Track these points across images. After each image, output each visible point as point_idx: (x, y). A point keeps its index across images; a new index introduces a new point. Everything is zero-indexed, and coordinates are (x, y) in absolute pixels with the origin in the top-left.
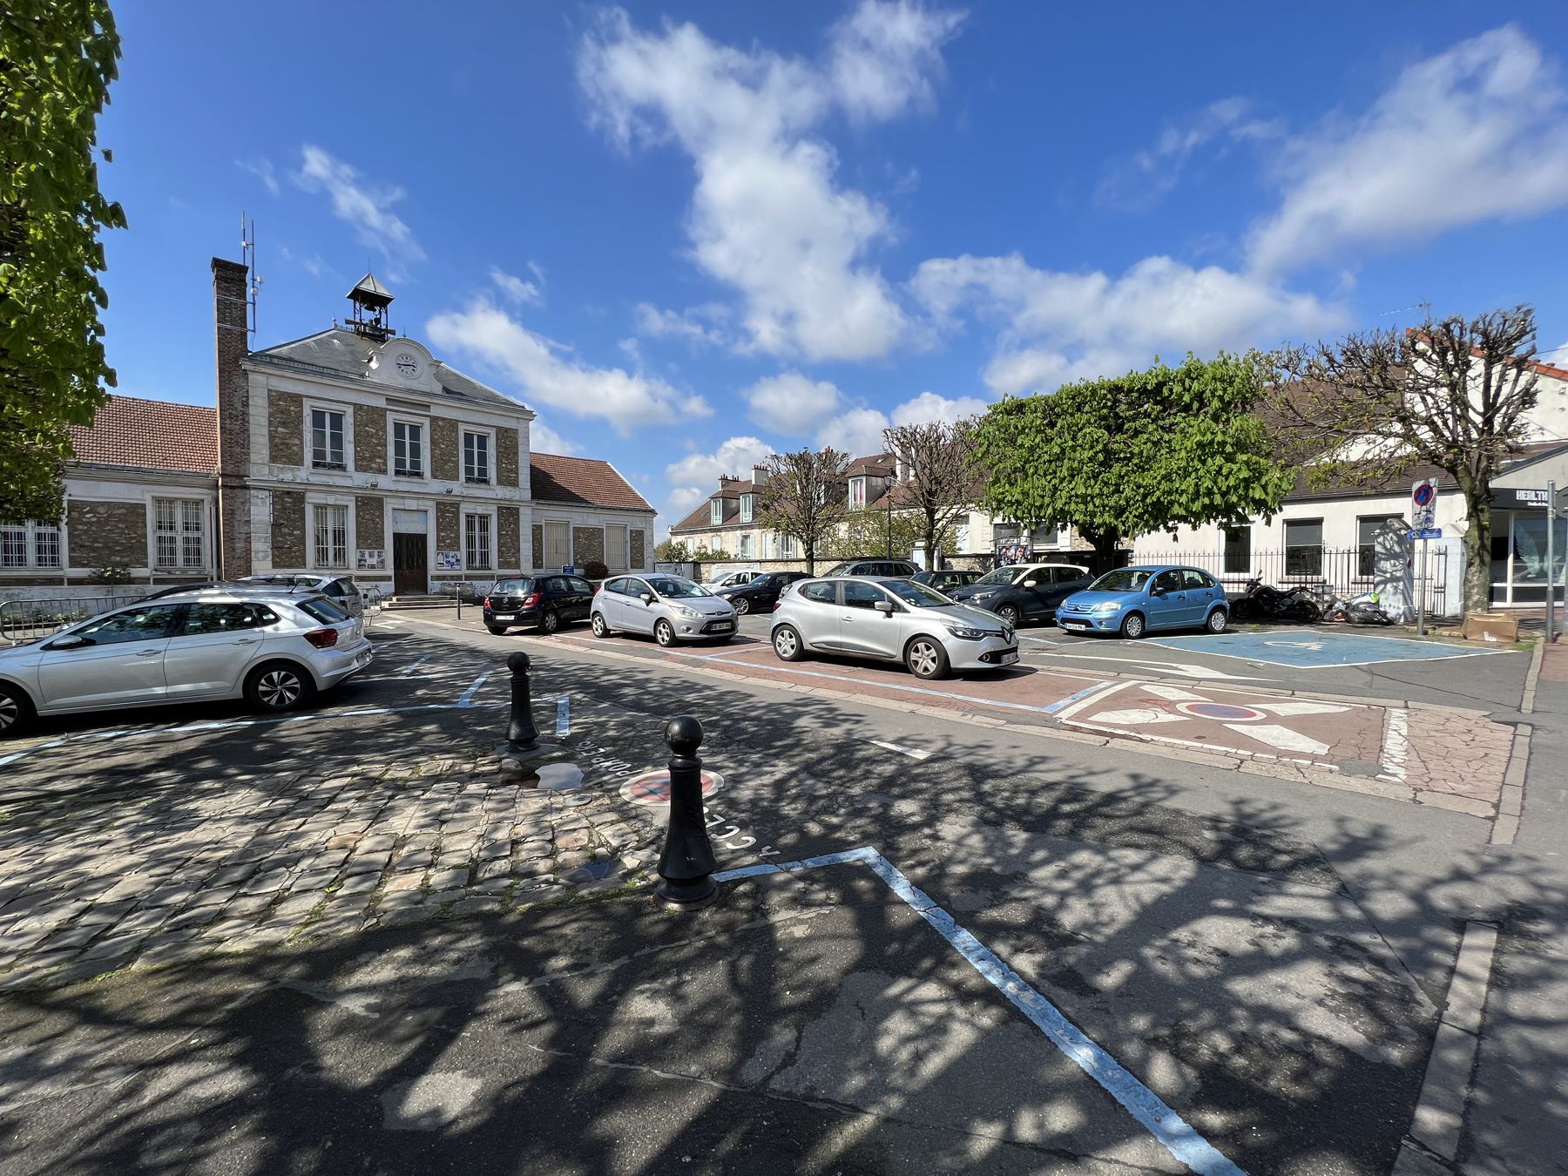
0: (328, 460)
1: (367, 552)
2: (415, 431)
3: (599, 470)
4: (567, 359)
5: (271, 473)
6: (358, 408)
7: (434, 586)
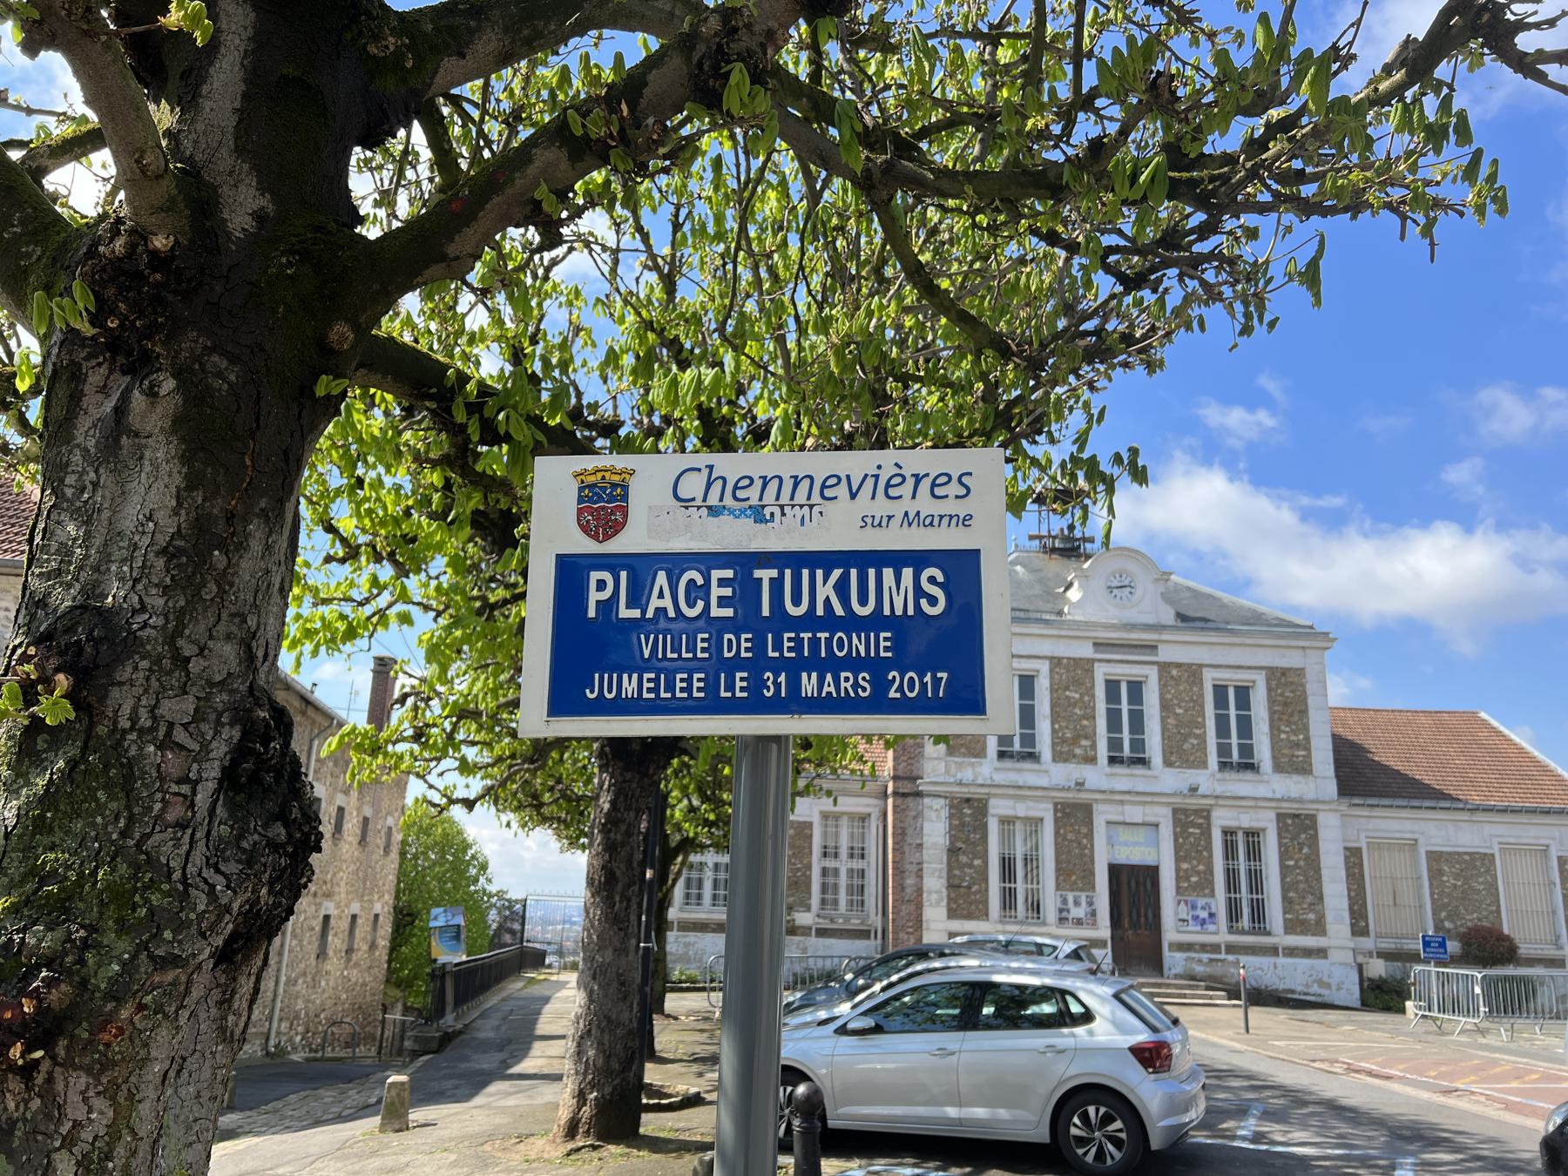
0: (1017, 746)
1: (1070, 897)
2: (1136, 689)
3: (1464, 730)
4: (1333, 523)
5: (947, 772)
6: (1056, 662)
7: (1174, 961)
